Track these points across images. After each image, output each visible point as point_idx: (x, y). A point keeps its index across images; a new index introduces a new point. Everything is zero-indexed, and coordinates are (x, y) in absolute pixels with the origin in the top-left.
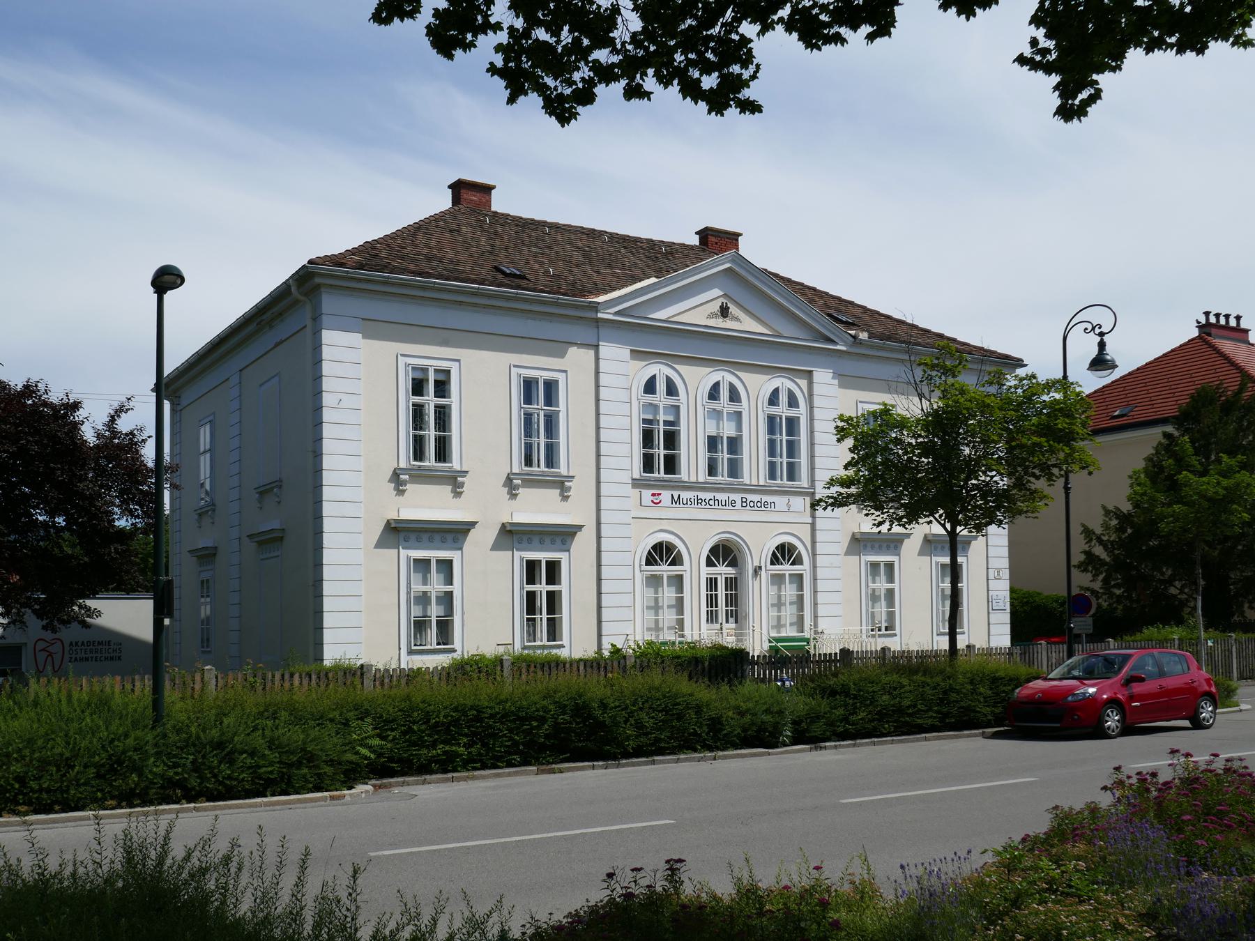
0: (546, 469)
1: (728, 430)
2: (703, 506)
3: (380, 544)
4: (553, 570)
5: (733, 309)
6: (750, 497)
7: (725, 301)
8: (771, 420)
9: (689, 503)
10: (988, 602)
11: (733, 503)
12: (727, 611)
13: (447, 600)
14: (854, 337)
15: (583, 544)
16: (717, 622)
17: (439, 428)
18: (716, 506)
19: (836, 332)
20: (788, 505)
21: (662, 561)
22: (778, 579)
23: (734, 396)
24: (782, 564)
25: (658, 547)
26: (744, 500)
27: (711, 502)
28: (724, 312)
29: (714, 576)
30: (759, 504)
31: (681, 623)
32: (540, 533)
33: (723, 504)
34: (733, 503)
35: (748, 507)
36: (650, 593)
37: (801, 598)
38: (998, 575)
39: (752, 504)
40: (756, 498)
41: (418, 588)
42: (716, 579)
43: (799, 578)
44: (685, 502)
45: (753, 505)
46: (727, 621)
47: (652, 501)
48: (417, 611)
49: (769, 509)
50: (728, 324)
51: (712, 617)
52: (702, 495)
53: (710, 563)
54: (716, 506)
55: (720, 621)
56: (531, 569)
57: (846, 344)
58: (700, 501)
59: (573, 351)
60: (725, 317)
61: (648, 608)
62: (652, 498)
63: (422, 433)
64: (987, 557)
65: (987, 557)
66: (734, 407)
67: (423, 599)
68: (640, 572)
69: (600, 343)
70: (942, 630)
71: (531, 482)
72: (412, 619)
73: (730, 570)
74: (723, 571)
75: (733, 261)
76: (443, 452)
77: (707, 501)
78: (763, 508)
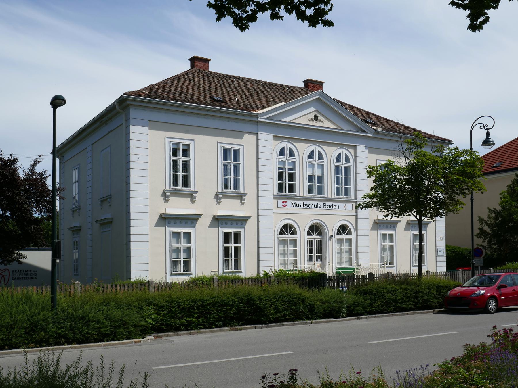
0: (234, 191)
1: (317, 172)
2: (306, 208)
3: (157, 225)
4: (237, 236)
5: (320, 117)
6: (328, 203)
7: (316, 113)
8: (337, 168)
9: (300, 206)
10: (436, 251)
11: (320, 206)
12: (317, 256)
13: (188, 250)
14: (375, 130)
15: (251, 224)
16: (312, 261)
17: (184, 171)
18: (312, 208)
19: (366, 127)
20: (345, 207)
21: (287, 233)
22: (340, 241)
23: (320, 157)
24: (286, 234)
25: (342, 227)
26: (325, 205)
27: (310, 206)
28: (316, 118)
29: (311, 240)
30: (332, 207)
31: (296, 261)
32: (227, 220)
33: (315, 206)
34: (320, 206)
35: (330, 208)
36: (282, 247)
37: (351, 250)
38: (441, 239)
39: (328, 207)
40: (330, 204)
41: (175, 245)
42: (312, 241)
43: (350, 241)
44: (298, 206)
45: (329, 207)
46: (317, 260)
47: (283, 205)
48: (174, 256)
49: (336, 209)
50: (318, 124)
51: (310, 258)
52: (306, 202)
53: (309, 234)
54: (312, 208)
55: (314, 260)
56: (227, 236)
57: (371, 133)
58: (305, 205)
59: (246, 136)
60: (316, 121)
61: (281, 254)
62: (283, 204)
63: (176, 173)
64: (436, 231)
65: (436, 231)
66: (320, 162)
67: (177, 250)
68: (277, 238)
69: (259, 132)
70: (415, 264)
71: (227, 196)
72: (172, 259)
73: (318, 237)
74: (315, 237)
75: (320, 95)
76: (186, 183)
77: (308, 205)
78: (334, 209)
